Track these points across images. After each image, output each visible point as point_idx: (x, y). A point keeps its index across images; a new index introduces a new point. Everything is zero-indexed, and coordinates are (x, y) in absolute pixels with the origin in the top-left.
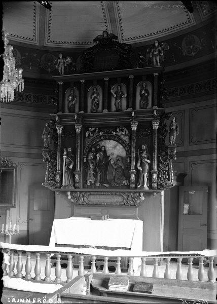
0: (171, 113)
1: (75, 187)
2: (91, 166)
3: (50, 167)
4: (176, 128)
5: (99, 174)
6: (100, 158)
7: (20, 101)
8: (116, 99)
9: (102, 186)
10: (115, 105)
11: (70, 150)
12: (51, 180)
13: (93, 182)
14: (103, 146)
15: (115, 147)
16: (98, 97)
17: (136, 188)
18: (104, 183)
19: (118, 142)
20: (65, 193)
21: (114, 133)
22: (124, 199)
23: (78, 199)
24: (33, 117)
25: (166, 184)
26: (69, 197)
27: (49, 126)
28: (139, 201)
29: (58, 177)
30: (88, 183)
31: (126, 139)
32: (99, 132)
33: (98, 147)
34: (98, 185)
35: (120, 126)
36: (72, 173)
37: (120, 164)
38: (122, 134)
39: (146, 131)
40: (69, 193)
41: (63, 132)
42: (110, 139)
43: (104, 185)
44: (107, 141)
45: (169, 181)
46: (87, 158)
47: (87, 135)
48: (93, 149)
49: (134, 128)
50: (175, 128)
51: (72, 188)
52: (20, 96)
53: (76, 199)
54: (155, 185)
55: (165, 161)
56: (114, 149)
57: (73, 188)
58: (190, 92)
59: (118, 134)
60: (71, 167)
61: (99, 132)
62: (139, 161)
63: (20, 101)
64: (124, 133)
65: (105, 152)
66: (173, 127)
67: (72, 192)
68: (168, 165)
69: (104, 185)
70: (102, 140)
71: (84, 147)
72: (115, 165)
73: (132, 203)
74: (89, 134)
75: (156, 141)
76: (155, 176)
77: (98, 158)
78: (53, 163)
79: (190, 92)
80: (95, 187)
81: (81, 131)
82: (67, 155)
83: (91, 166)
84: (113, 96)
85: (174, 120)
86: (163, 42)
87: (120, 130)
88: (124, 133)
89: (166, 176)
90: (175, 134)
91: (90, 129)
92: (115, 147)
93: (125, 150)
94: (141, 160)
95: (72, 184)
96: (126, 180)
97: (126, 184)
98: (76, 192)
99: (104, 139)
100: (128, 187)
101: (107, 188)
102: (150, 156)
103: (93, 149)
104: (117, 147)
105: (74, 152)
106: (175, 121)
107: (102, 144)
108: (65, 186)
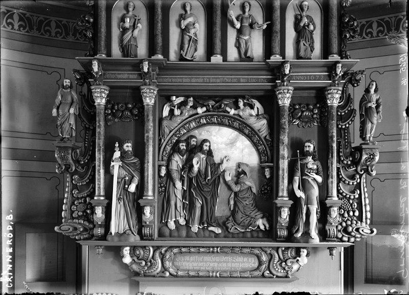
0: (362, 72)
1: (142, 237)
2: (179, 184)
3: (75, 187)
4: (377, 107)
5: (198, 204)
6: (199, 169)
7: (60, 38)
8: (240, 32)
9: (204, 233)
10: (238, 47)
11: (128, 147)
12: (79, 217)
13: (182, 222)
14: (205, 141)
15: (232, 143)
16: (197, 25)
17: (290, 238)
18: (210, 225)
19: (240, 131)
20: (116, 252)
21: (232, 112)
22: (260, 263)
23: (151, 264)
24: (27, 66)
25: (357, 230)
26: (127, 260)
27: (71, 87)
28: (295, 267)
29: (99, 213)
30: (172, 225)
31: (261, 125)
32: (194, 107)
33: (193, 142)
34: (195, 228)
35: (247, 96)
36: (136, 205)
37: (248, 183)
38: (251, 115)
39: (308, 110)
40: (126, 251)
41: (108, 102)
42: (221, 124)
43: (211, 228)
44: (214, 129)
45: (362, 221)
46: (167, 166)
47: (166, 112)
48: (183, 146)
49: (285, 100)
50: (374, 106)
51: (135, 239)
52: (24, 21)
53: (144, 263)
54: (332, 230)
55: (352, 177)
56: (232, 149)
57: (138, 237)
58: (364, 35)
59: (241, 114)
60: (132, 188)
61: (194, 107)
62: (297, 179)
63: (60, 38)
64: (254, 112)
65: (210, 153)
66: (369, 105)
67: (133, 249)
68: (359, 186)
69: (211, 228)
70: (201, 126)
71: (160, 140)
72: (237, 183)
73: (281, 273)
74: (172, 112)
75: (335, 134)
76: (334, 213)
77: (196, 168)
78: (82, 177)
79: (364, 35)
80: (189, 236)
81: (155, 101)
82: (122, 158)
83: (179, 184)
84: (233, 25)
85: (374, 87)
86: (86, 131)
87: (245, 105)
88: (254, 112)
89: (354, 212)
90: (375, 120)
91: (174, 98)
92: (232, 143)
93: (258, 150)
94: (303, 174)
95: (135, 230)
96: (262, 218)
97: (262, 227)
98: (144, 247)
99: (208, 124)
100: (270, 234)
101: (217, 235)
102: (321, 169)
103: (183, 146)
104: (239, 144)
105: (140, 151)
106: (376, 91)
107: (201, 134)
108: (118, 234)
